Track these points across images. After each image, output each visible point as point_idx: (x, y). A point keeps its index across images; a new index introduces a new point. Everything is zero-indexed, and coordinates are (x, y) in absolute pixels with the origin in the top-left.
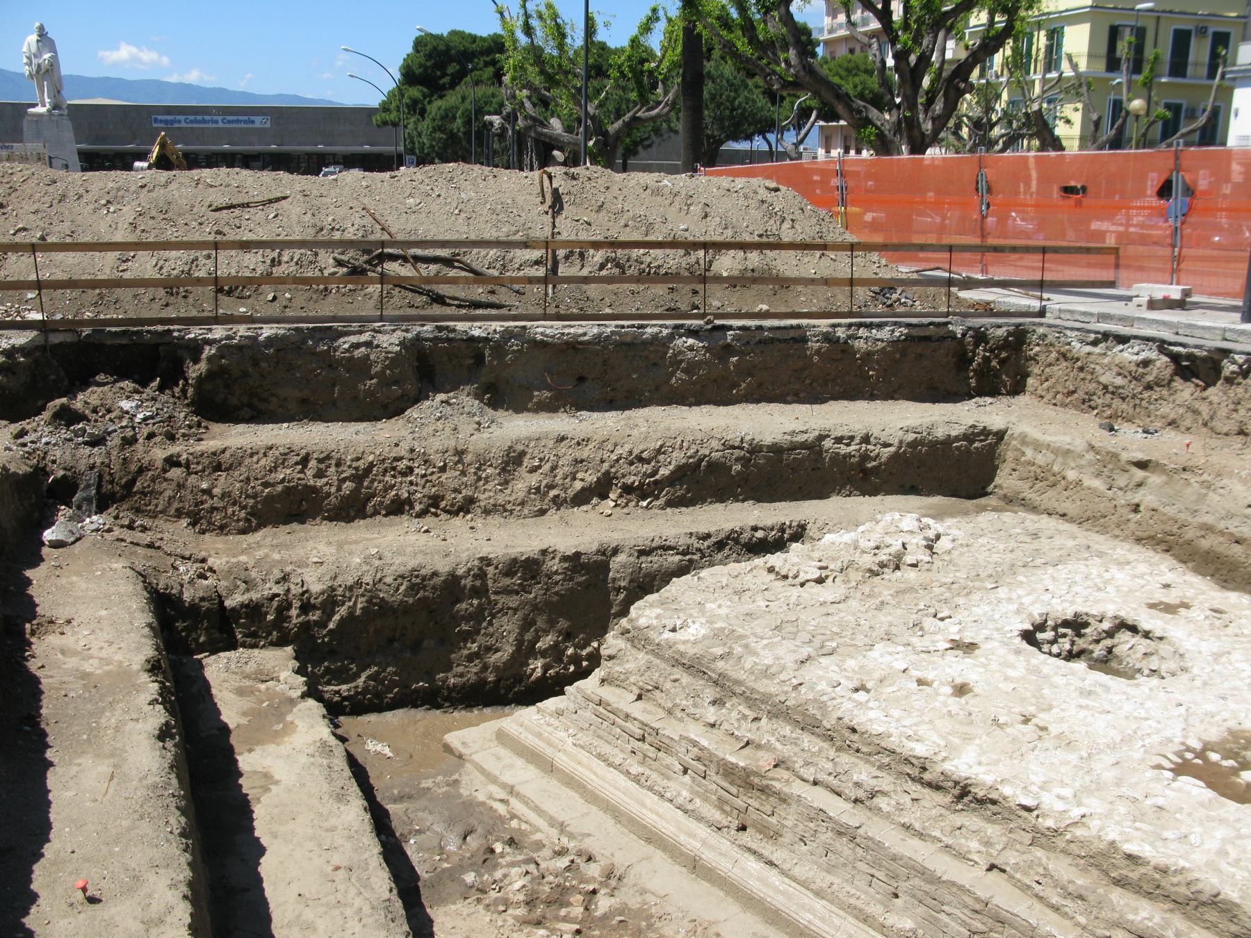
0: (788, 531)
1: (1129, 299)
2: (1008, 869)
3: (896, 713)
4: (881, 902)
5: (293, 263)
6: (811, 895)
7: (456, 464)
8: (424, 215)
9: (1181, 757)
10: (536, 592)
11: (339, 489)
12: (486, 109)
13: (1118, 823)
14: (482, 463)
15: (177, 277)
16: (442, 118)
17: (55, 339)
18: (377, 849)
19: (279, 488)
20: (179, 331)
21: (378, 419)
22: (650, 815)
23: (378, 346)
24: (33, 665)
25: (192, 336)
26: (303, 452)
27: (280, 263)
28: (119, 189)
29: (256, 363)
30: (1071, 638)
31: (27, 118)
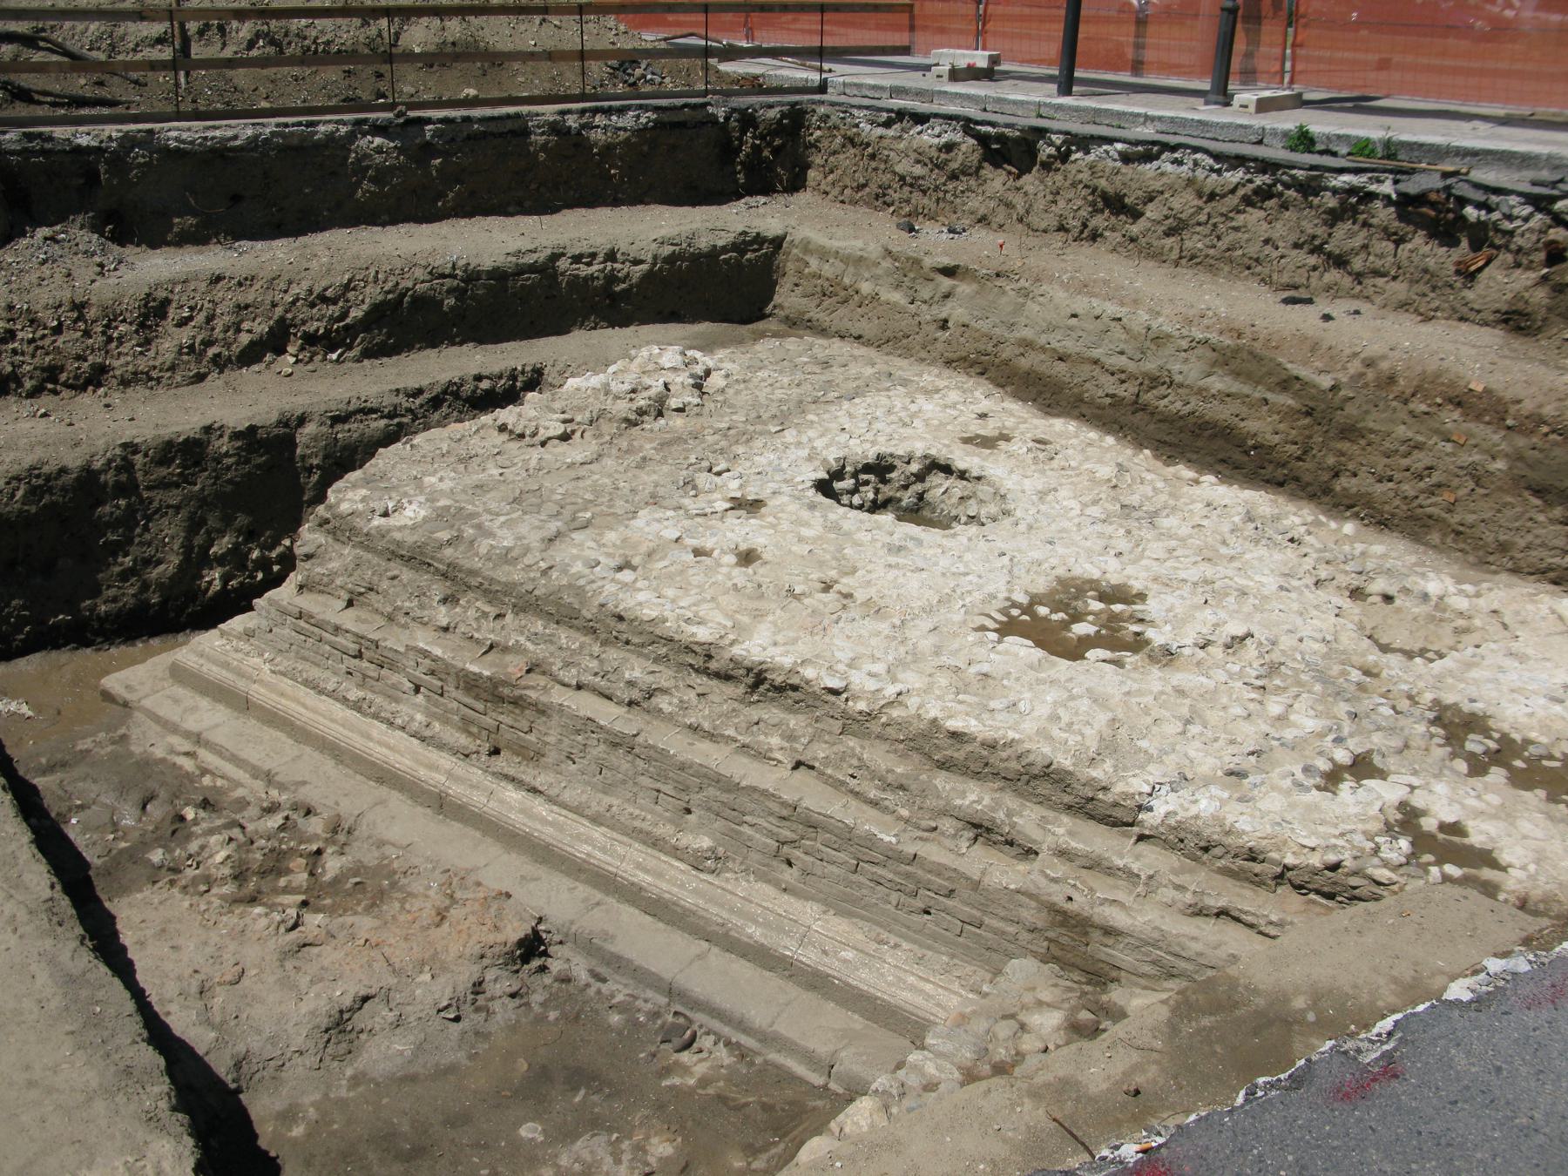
0: (521, 378)
1: (928, 68)
2: (817, 765)
3: (670, 592)
4: (670, 821)
7: (75, 321)
9: (1007, 614)
10: (202, 482)
13: (939, 698)
14: (112, 318)
18: (26, 836)
22: (378, 749)
30: (881, 486)
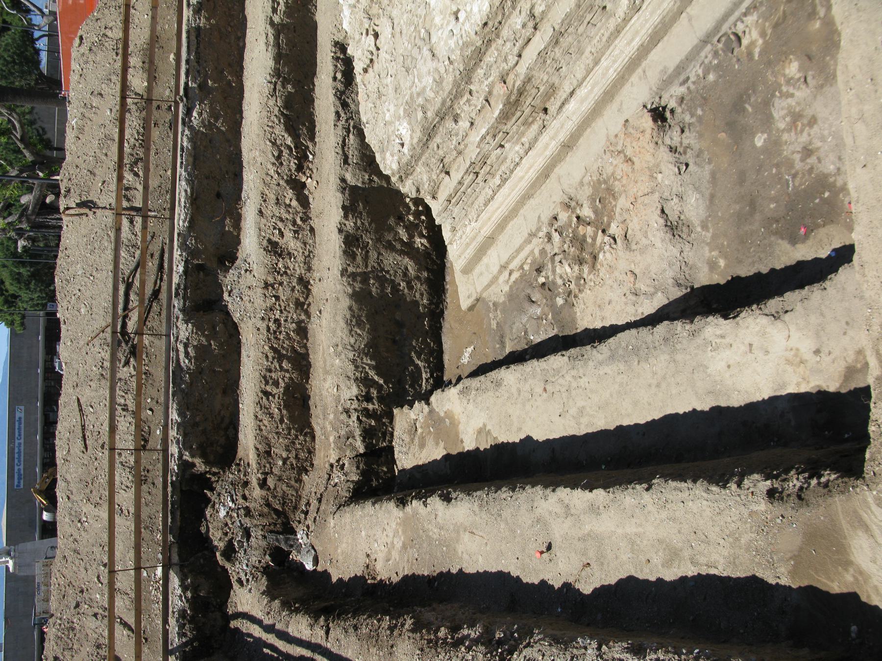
0: (338, 55)
4: (607, 19)
5: (126, 396)
6: (597, 68)
8: (94, 302)
10: (368, 239)
11: (287, 371)
12: (12, 250)
14: (275, 270)
15: (134, 476)
16: (19, 282)
17: (175, 558)
18: (534, 363)
19: (284, 412)
20: (172, 476)
21: (239, 342)
22: (530, 174)
23: (188, 339)
24: (395, 579)
25: (176, 468)
26: (260, 394)
27: (125, 405)
28: (70, 514)
29: (196, 425)
31: (17, 572)
